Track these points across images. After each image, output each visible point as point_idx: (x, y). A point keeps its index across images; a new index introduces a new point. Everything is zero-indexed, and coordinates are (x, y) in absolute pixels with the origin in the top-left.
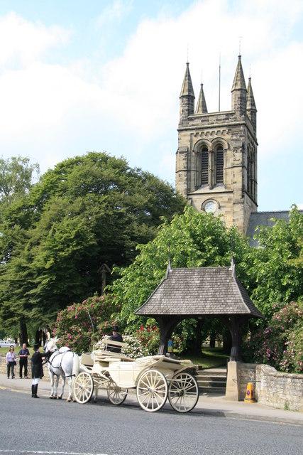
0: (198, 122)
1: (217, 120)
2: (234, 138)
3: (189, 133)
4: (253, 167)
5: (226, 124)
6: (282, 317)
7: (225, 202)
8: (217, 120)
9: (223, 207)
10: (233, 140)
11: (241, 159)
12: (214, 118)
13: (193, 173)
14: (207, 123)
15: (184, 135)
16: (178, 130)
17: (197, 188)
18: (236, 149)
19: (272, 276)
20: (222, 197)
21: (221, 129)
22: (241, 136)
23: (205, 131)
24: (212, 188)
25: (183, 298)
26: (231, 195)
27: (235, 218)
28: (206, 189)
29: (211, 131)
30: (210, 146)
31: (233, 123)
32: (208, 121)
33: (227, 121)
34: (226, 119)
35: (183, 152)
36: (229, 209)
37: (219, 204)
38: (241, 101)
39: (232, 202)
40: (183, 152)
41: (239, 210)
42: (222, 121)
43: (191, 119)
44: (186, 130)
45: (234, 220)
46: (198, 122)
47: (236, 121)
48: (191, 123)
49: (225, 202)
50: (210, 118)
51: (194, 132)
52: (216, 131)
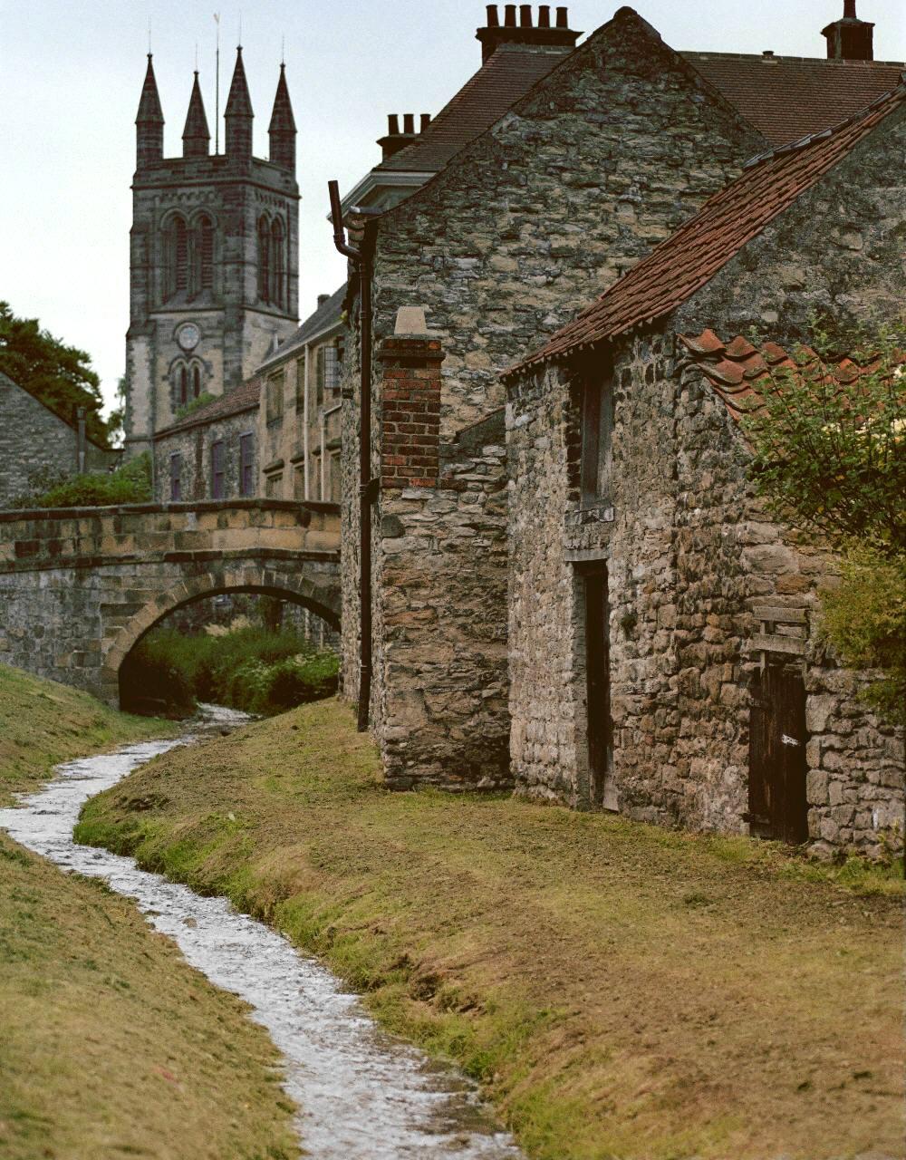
5: (213, 180)
17: (165, 300)
20: (206, 319)
23: (180, 191)
32: (184, 172)
45: (225, 363)
52: (197, 193)
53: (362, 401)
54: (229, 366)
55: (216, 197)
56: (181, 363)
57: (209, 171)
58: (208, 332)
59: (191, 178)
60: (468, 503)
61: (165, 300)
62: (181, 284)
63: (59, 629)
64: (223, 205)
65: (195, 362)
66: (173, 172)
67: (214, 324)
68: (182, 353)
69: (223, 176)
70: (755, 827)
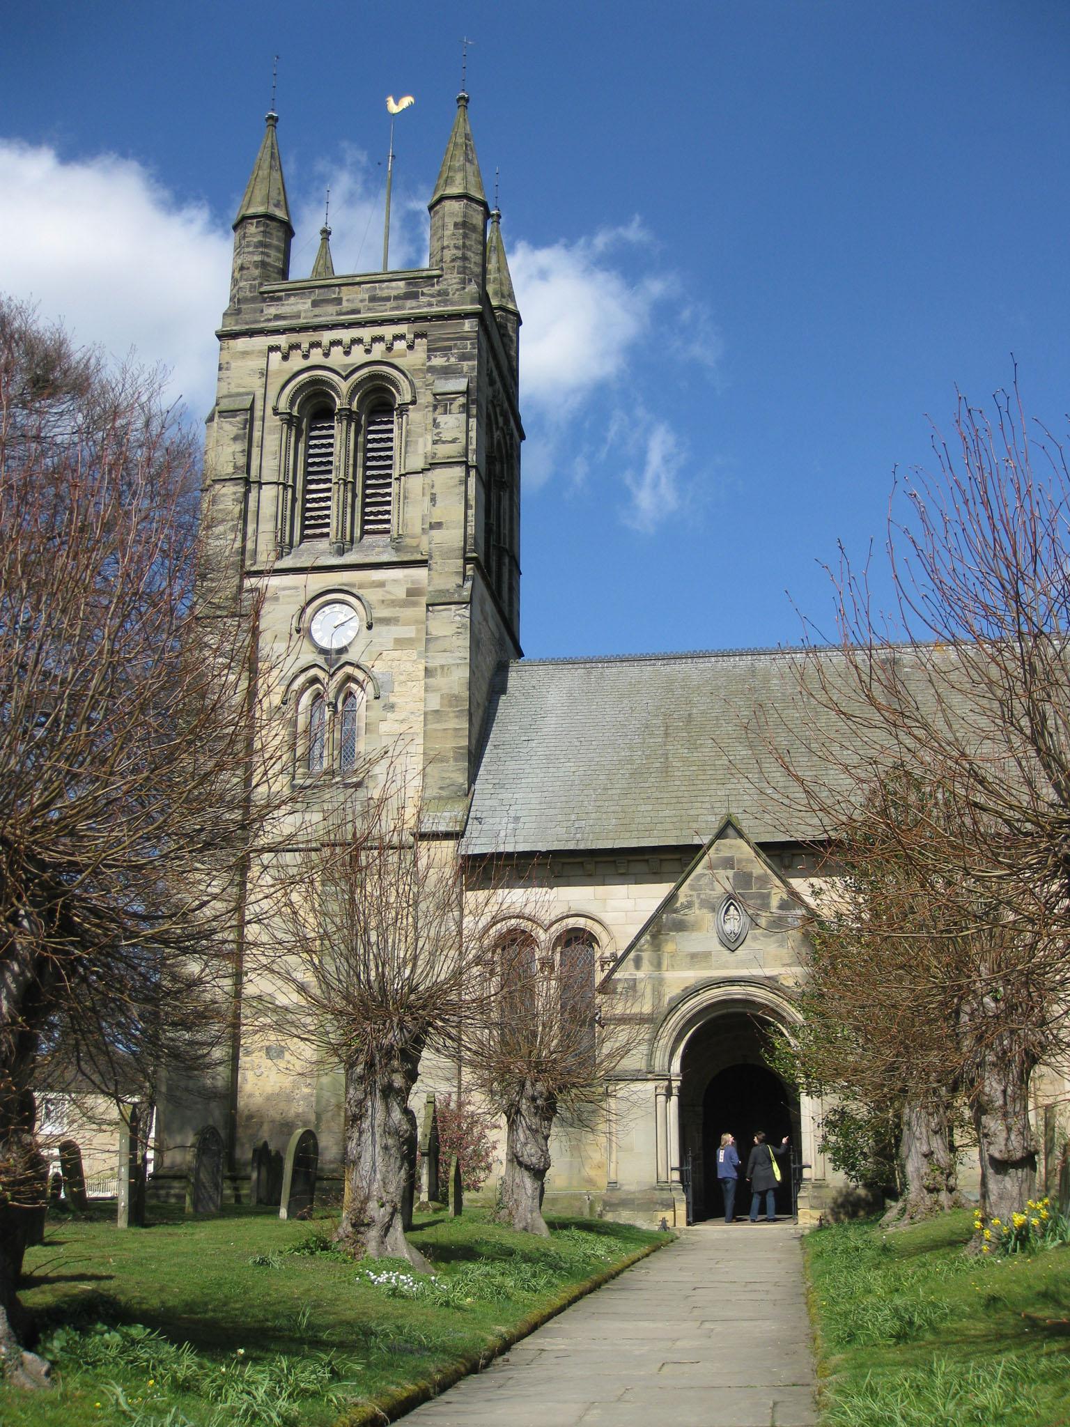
0: (300, 307)
1: (373, 299)
2: (438, 361)
3: (263, 342)
4: (505, 503)
5: (405, 312)
6: (894, 1353)
7: (394, 603)
8: (373, 299)
9: (386, 621)
10: (431, 369)
11: (462, 437)
12: (362, 293)
13: (269, 493)
14: (332, 309)
15: (245, 354)
16: (221, 336)
17: (284, 549)
18: (441, 402)
19: (882, 746)
20: (382, 584)
21: (388, 331)
22: (463, 357)
23: (327, 337)
24: (341, 552)
25: (392, 1046)
26: (420, 573)
27: (437, 661)
28: (320, 551)
29: (346, 335)
30: (343, 393)
31: (436, 309)
32: (338, 301)
33: (410, 303)
34: (413, 296)
35: (233, 413)
36: (409, 632)
37: (368, 607)
38: (465, 236)
39: (424, 600)
40: (233, 413)
41: (449, 630)
42: (392, 304)
43: (273, 298)
44: (251, 333)
45: (428, 672)
46: (300, 307)
47: (445, 302)
48: (272, 310)
49: (394, 603)
50: (346, 293)
51: (282, 340)
52: (367, 339)
53: (655, 876)
54: (438, 681)
55: (411, 347)
56: (315, 680)
57: (396, 298)
58: (380, 613)
59: (357, 311)
60: (383, 1180)
61: (284, 549)
62: (313, 527)
63: (834, 1355)
64: (429, 358)
65: (350, 678)
66: (315, 304)
67: (401, 594)
68: (320, 660)
69: (430, 305)
70: (70, 1141)
